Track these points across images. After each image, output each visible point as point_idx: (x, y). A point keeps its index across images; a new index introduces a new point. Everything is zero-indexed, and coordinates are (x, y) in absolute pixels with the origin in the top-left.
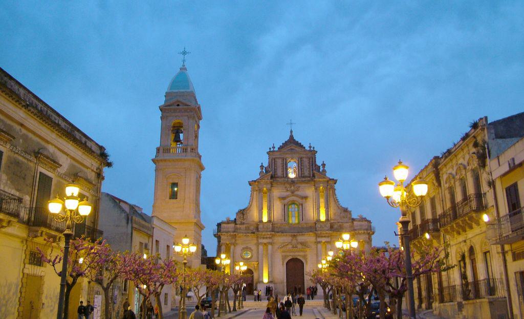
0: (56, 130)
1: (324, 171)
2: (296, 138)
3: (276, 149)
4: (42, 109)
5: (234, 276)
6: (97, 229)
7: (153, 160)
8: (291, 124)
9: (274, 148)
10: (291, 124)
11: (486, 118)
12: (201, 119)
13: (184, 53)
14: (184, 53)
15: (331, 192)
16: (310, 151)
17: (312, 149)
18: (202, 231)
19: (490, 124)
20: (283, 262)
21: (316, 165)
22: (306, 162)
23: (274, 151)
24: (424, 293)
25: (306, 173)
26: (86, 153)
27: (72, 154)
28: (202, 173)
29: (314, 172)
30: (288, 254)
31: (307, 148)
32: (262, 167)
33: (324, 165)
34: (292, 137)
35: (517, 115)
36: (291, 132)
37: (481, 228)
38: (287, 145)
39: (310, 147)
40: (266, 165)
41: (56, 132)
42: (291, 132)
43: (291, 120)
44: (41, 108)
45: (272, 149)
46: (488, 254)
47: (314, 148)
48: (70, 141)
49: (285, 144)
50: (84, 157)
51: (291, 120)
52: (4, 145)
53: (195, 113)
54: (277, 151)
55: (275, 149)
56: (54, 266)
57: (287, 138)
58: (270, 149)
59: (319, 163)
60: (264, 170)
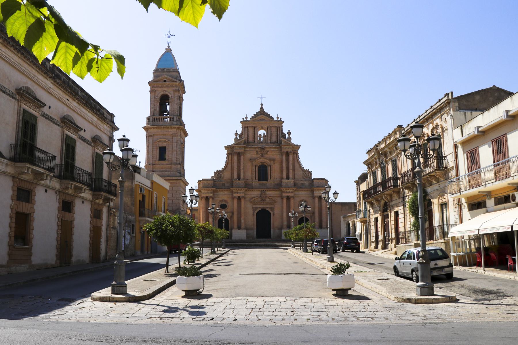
0: (77, 99)
1: (290, 138)
2: (266, 110)
3: (249, 119)
4: (65, 80)
5: (412, 194)
6: (111, 183)
7: (144, 128)
8: (262, 98)
9: (246, 118)
10: (262, 98)
11: (452, 93)
12: (184, 93)
13: (169, 36)
14: (169, 36)
15: (295, 155)
16: (278, 121)
17: (279, 119)
18: (187, 187)
19: (456, 98)
20: (254, 213)
21: (283, 133)
22: (274, 130)
23: (246, 121)
24: (380, 237)
25: (274, 139)
26: (100, 119)
27: (90, 119)
28: (186, 138)
29: (281, 138)
30: (258, 206)
31: (275, 119)
32: (236, 134)
33: (289, 133)
34: (262, 108)
35: (486, 89)
36: (262, 105)
37: (439, 184)
38: (258, 116)
39: (278, 118)
40: (240, 132)
41: (76, 101)
42: (262, 105)
43: (261, 95)
44: (64, 79)
45: (245, 120)
46: (444, 207)
47: (281, 119)
48: (88, 108)
49: (256, 115)
50: (99, 122)
51: (261, 95)
52: (37, 111)
53: (180, 88)
54: (249, 121)
55: (247, 119)
56: (447, 156)
57: (258, 110)
58: (243, 119)
59: (285, 131)
60: (238, 137)
